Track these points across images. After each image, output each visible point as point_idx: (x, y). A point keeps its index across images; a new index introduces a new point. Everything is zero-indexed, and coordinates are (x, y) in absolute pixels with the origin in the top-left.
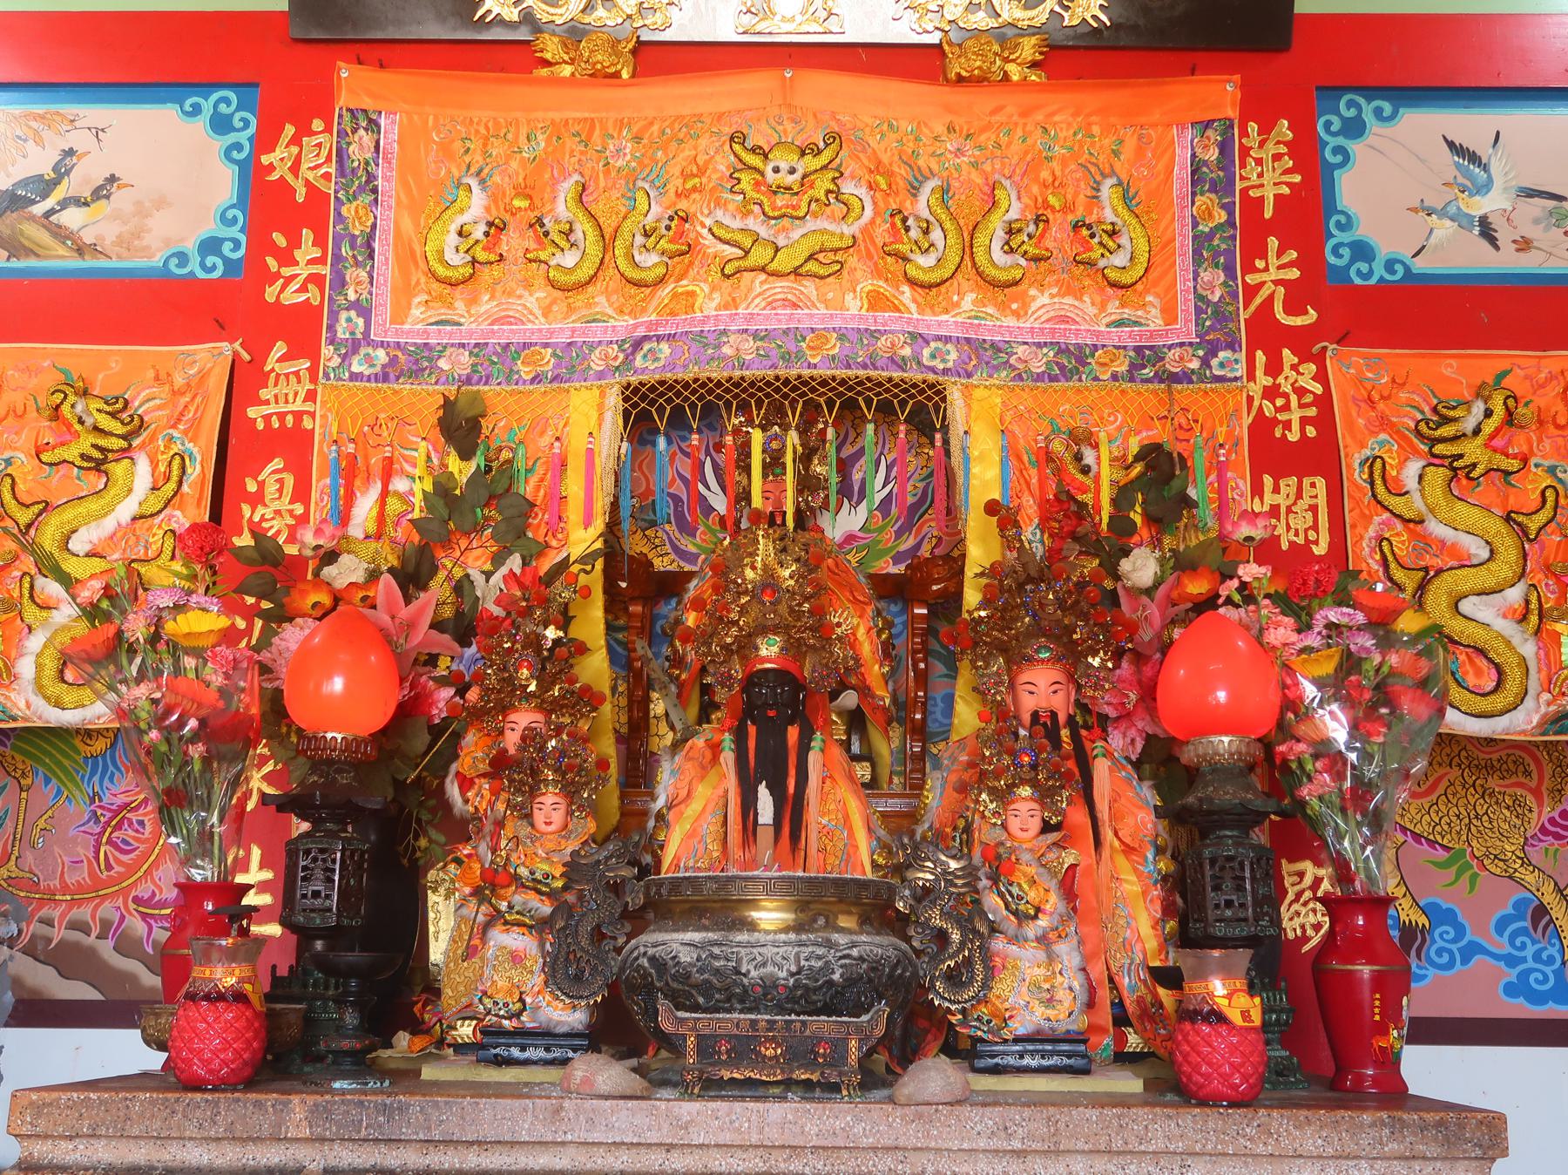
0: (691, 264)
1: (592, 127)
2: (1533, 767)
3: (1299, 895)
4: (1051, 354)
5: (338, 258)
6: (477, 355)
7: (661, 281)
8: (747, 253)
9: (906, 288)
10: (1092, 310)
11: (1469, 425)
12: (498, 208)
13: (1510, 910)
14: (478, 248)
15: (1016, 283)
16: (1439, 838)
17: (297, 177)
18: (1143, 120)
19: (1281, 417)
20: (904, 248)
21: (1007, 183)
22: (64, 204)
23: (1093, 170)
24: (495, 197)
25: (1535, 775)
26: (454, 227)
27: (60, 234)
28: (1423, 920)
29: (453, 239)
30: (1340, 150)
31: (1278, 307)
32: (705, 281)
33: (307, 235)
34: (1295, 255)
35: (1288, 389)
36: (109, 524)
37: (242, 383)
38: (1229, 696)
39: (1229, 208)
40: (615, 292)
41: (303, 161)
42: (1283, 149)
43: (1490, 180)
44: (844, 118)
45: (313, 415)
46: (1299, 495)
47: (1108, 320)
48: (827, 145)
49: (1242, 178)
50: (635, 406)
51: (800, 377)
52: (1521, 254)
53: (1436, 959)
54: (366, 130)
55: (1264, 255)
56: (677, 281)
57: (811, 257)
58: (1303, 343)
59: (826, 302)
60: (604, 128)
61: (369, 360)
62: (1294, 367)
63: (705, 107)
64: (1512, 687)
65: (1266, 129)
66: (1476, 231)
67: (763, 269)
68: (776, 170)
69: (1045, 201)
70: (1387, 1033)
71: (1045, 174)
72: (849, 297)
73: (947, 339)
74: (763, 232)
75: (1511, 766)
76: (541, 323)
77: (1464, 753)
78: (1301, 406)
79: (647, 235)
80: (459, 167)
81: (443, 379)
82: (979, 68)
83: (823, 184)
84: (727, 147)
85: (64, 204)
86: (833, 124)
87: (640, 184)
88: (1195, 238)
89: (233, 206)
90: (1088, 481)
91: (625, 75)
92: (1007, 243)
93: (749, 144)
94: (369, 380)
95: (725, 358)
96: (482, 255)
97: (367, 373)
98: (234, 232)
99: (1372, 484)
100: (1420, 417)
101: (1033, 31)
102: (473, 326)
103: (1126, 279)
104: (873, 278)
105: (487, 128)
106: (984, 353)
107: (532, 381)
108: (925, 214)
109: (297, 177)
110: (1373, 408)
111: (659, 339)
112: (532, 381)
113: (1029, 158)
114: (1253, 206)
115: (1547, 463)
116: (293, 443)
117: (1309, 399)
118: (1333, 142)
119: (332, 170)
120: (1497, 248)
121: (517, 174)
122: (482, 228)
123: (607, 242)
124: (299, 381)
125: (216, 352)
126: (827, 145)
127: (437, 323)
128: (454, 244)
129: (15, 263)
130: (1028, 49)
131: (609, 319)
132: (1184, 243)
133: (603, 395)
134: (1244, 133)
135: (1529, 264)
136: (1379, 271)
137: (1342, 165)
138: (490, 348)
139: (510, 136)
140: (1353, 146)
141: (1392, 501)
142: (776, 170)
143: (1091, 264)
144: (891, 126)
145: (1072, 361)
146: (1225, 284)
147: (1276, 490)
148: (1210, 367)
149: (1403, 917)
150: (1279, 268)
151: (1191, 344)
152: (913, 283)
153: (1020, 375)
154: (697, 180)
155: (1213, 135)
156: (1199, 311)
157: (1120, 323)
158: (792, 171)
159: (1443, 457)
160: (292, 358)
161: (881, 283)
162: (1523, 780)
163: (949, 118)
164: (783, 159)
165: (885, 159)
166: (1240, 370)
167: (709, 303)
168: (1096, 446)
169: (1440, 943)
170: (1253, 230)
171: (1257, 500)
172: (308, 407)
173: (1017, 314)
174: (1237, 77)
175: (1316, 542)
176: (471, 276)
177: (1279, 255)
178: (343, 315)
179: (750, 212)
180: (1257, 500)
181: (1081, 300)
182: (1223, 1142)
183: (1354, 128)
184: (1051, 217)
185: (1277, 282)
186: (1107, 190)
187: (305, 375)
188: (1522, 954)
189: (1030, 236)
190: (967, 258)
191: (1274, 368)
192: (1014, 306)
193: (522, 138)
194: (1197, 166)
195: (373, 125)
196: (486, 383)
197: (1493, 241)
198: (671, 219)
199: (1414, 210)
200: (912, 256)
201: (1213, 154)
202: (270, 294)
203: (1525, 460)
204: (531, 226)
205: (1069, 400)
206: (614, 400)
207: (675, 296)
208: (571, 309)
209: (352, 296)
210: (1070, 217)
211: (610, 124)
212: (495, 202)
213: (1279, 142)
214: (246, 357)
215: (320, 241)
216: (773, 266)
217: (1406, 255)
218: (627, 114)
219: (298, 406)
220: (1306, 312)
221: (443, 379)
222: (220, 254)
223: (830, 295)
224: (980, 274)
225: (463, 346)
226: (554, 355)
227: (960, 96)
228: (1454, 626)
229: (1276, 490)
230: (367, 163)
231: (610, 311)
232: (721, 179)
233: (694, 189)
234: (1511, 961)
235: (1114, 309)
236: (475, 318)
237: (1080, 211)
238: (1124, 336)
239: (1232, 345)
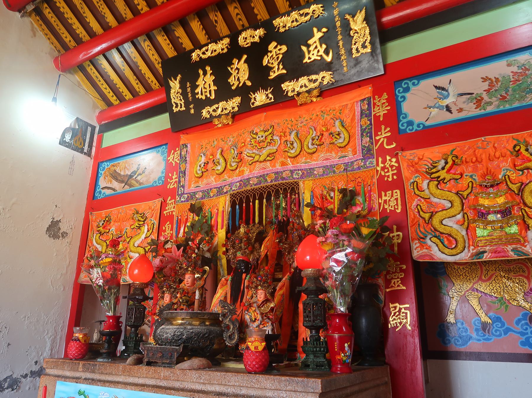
2: (525, 269)
3: (395, 313)
7: (237, 168)
9: (289, 159)
11: (440, 167)
13: (521, 317)
16: (493, 294)
19: (387, 174)
22: (138, 175)
25: (526, 272)
27: (137, 181)
28: (489, 321)
29: (199, 168)
31: (385, 145)
33: (175, 173)
35: (388, 166)
36: (141, 240)
38: (310, 258)
43: (449, 94)
46: (392, 196)
49: (374, 111)
52: (460, 113)
53: (494, 333)
55: (380, 131)
57: (268, 156)
58: (393, 153)
62: (390, 160)
64: (460, 246)
65: (380, 96)
66: (445, 109)
70: (340, 355)
74: (257, 152)
75: (518, 270)
77: (500, 267)
78: (392, 170)
83: (270, 138)
85: (138, 175)
88: (361, 130)
90: (332, 201)
91: (230, 123)
99: (414, 189)
100: (427, 167)
106: (308, 173)
108: (293, 140)
114: (377, 118)
115: (470, 174)
116: (170, 217)
117: (394, 168)
118: (400, 95)
120: (452, 113)
122: (203, 164)
129: (131, 189)
130: (315, 93)
134: (374, 99)
135: (462, 115)
136: (415, 127)
137: (403, 101)
140: (407, 95)
141: (422, 194)
143: (333, 143)
147: (386, 195)
149: (482, 320)
152: (289, 157)
155: (366, 102)
156: (363, 150)
158: (262, 137)
159: (435, 178)
162: (522, 274)
166: (375, 163)
167: (247, 173)
168: (334, 191)
169: (496, 328)
171: (380, 199)
175: (397, 209)
177: (385, 129)
180: (380, 199)
182: (248, 384)
188: (527, 332)
191: (384, 162)
194: (362, 111)
197: (450, 112)
199: (426, 108)
203: (462, 175)
206: (228, 198)
207: (240, 172)
217: (423, 121)
219: (173, 210)
228: (441, 229)
229: (386, 195)
234: (523, 334)
236: (203, 184)
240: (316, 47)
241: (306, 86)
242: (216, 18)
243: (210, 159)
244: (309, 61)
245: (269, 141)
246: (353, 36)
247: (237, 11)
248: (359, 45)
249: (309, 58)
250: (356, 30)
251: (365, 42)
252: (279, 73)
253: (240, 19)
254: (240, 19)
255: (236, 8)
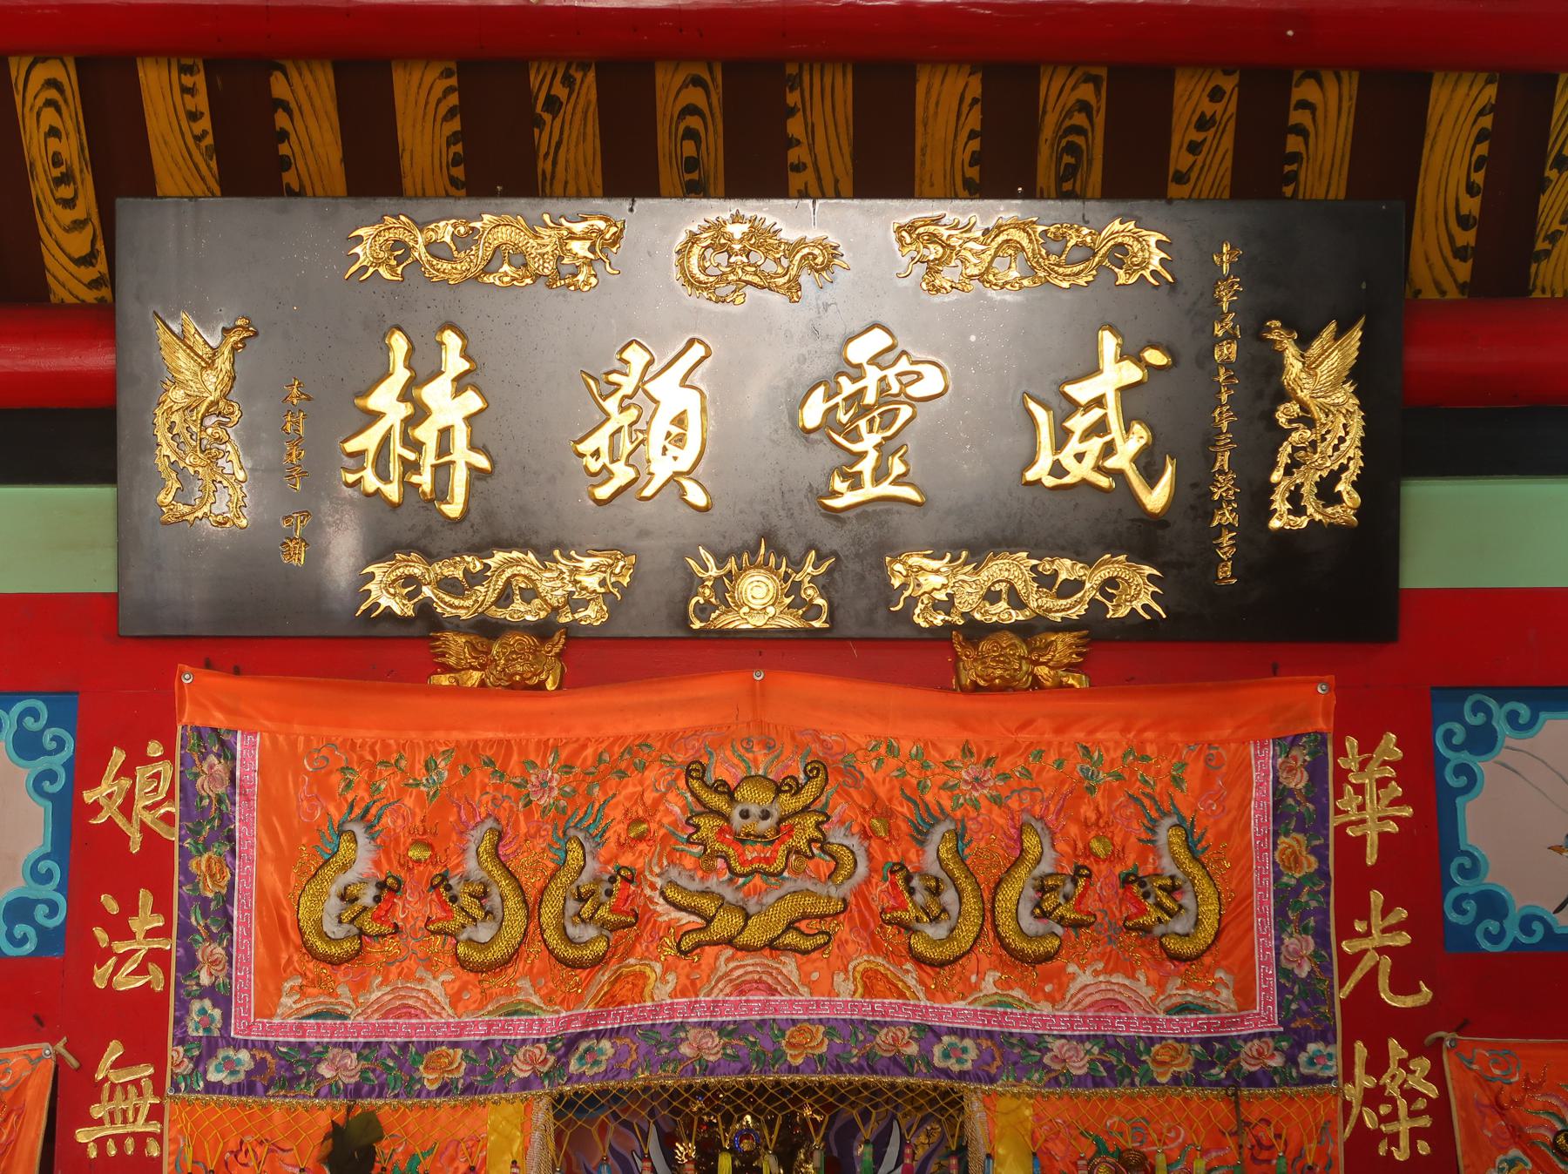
0: (638, 937)
1: (508, 755)
4: (1096, 1050)
5: (186, 930)
6: (366, 1058)
7: (599, 961)
8: (709, 921)
10: (1148, 992)
12: (389, 861)
14: (367, 916)
15: (1049, 957)
17: (129, 819)
18: (1210, 736)
20: (908, 915)
21: (1038, 826)
23: (1147, 802)
24: (386, 846)
26: (335, 889)
29: (333, 904)
30: (1463, 770)
31: (1383, 982)
32: (657, 959)
33: (145, 898)
34: (1405, 914)
35: (1396, 1093)
37: (71, 1096)
39: (1319, 853)
40: (542, 974)
41: (137, 796)
42: (1390, 772)
44: (831, 738)
45: (159, 1138)
47: (1168, 1003)
48: (809, 779)
50: (568, 1124)
51: (778, 1083)
54: (218, 756)
55: (1365, 916)
56: (622, 959)
57: (790, 926)
58: (1416, 1032)
59: (812, 987)
60: (523, 751)
61: (230, 1065)
62: (1403, 1064)
63: (652, 725)
65: (1367, 746)
67: (730, 942)
68: (745, 815)
69: (1087, 848)
71: (1087, 811)
72: (839, 978)
73: (963, 1033)
74: (729, 894)
76: (448, 1016)
78: (1413, 1114)
79: (581, 899)
80: (338, 808)
81: (324, 1091)
82: (1001, 677)
84: (682, 783)
86: (816, 747)
87: (572, 832)
89: (45, 857)
91: (550, 686)
92: (1038, 905)
93: (710, 778)
94: (230, 1092)
95: (683, 1058)
96: (372, 927)
97: (226, 1082)
98: (49, 891)
100: (1559, 1127)
101: (1067, 626)
102: (360, 1019)
103: (1187, 948)
104: (869, 952)
105: (373, 753)
106: (1014, 1054)
107: (439, 1092)
108: (935, 869)
109: (129, 819)
110: (1502, 1116)
111: (600, 1035)
112: (439, 1092)
113: (1066, 788)
117: (1421, 1104)
118: (1455, 758)
119: (174, 809)
121: (414, 814)
123: (532, 910)
124: (140, 1094)
125: (34, 1055)
126: (809, 779)
127: (315, 1015)
128: (335, 913)
131: (537, 1012)
132: (1264, 902)
133: (528, 1109)
134: (1341, 751)
137: (1467, 790)
138: (385, 1049)
139: (403, 763)
140: (1483, 766)
142: (745, 815)
143: (1146, 929)
144: (890, 748)
145: (1121, 1060)
146: (1315, 955)
148: (1296, 1064)
150: (1385, 931)
151: (1272, 1034)
152: (919, 960)
153: (1056, 1078)
154: (645, 826)
155: (1302, 755)
156: (1281, 989)
157: (1183, 1008)
158: (765, 815)
160: (135, 1063)
161: (880, 960)
163: (966, 735)
164: (753, 798)
165: (882, 792)
166: (1335, 1068)
167: (662, 988)
170: (1351, 880)
172: (154, 1127)
173: (1050, 998)
174: (1331, 678)
176: (358, 953)
177: (1385, 912)
178: (196, 1006)
179: (711, 870)
181: (1133, 977)
183: (1482, 740)
184: (1095, 868)
185: (1381, 950)
186: (1166, 833)
187: (147, 1085)
189: (1067, 898)
190: (988, 927)
191: (1377, 1065)
192: (1048, 988)
193: (419, 766)
195: (227, 752)
196: (380, 1096)
198: (612, 880)
200: (918, 926)
201: (1299, 781)
202: (100, 977)
204: (435, 887)
205: (1118, 1112)
206: (542, 1114)
208: (486, 997)
209: (205, 979)
210: (1118, 869)
211: (532, 747)
212: (387, 853)
213: (1385, 763)
214: (73, 1062)
215: (162, 906)
216: (743, 939)
217: (1546, 908)
218: (551, 735)
219: (140, 1127)
220: (1418, 991)
221: (324, 1091)
222: (31, 921)
223: (815, 976)
224: (1005, 946)
225: (349, 1045)
226: (465, 1056)
227: (979, 705)
230: (220, 800)
231: (536, 1000)
232: (674, 823)
233: (641, 838)
235: (1176, 991)
236: (366, 1007)
237: (1131, 859)
238: (1193, 1028)
239: (1326, 1036)
240: (1100, 428)
241: (1017, 602)
242: (560, 91)
243: (409, 865)
244: (1050, 482)
245: (803, 845)
246: (1287, 433)
247: (695, 96)
248: (1308, 481)
249: (1058, 470)
250: (1304, 407)
251: (1335, 477)
252: (886, 489)
253: (691, 134)
254: (691, 134)
255: (697, 82)
